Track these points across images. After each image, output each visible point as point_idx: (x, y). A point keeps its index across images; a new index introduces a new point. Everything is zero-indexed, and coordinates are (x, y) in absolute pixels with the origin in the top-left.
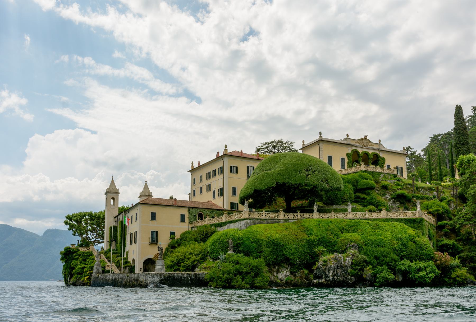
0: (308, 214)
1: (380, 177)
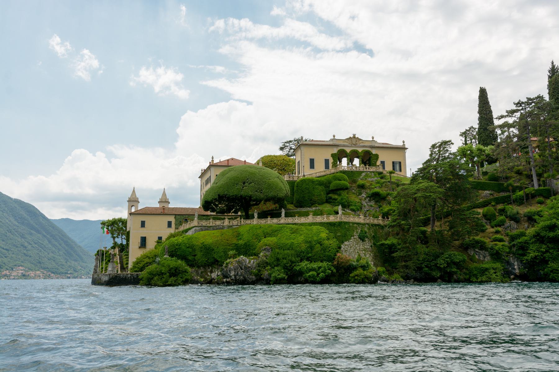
1: (362, 175)
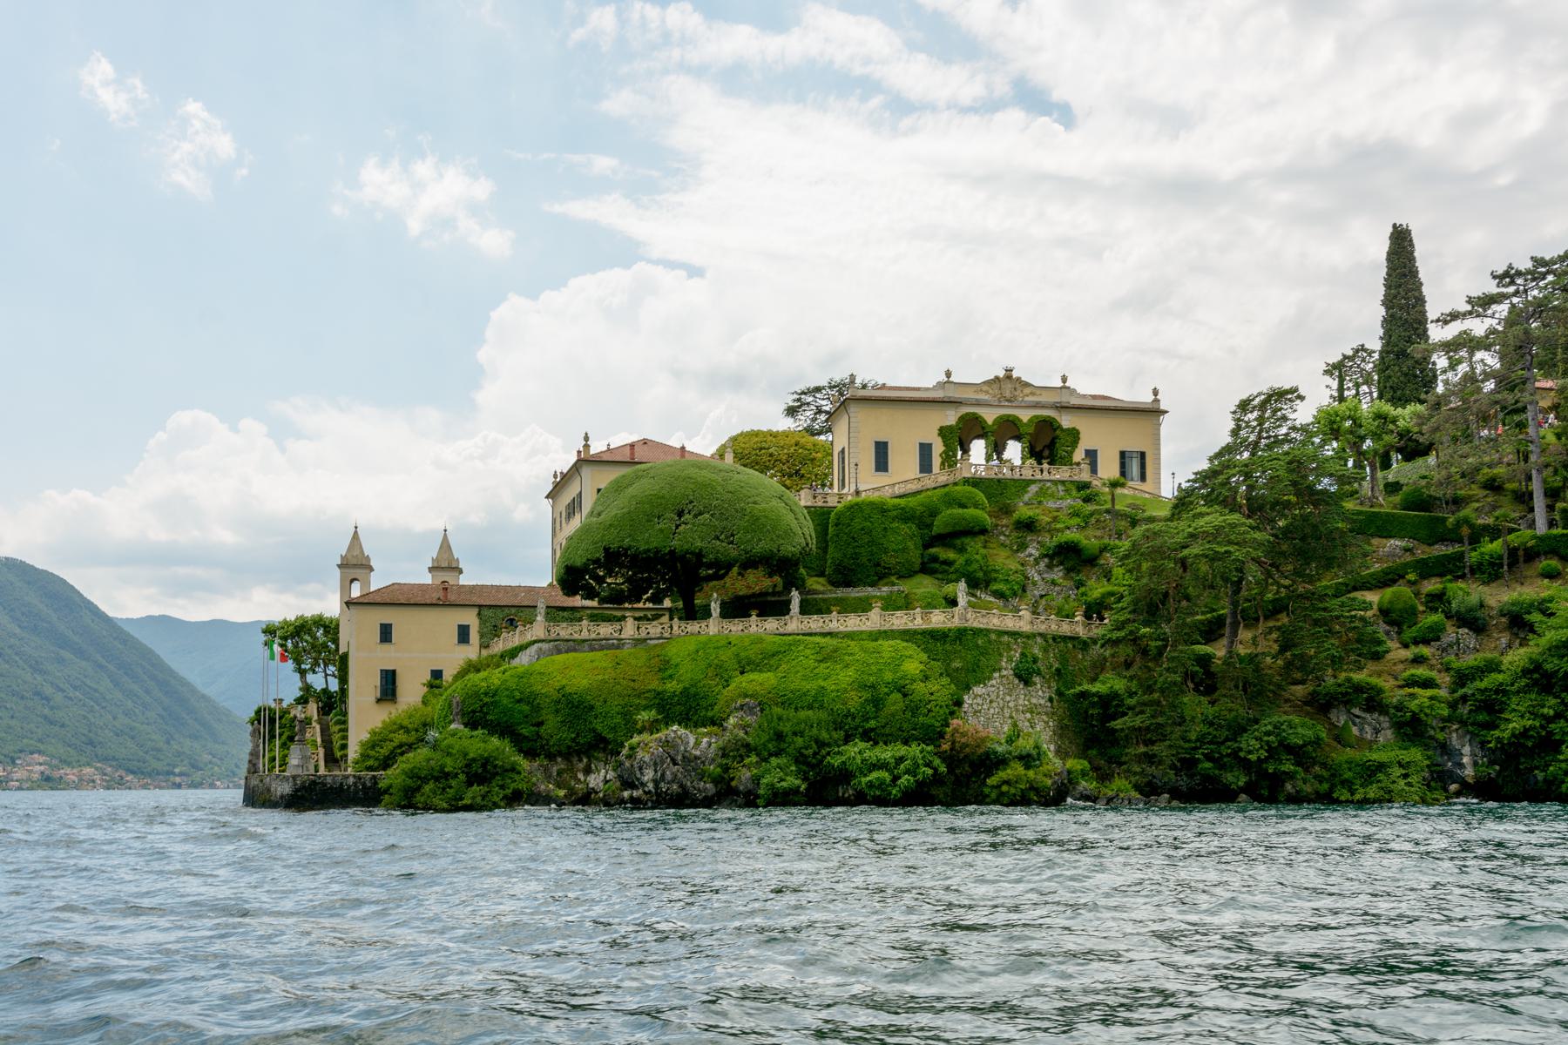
0: (695, 623)
